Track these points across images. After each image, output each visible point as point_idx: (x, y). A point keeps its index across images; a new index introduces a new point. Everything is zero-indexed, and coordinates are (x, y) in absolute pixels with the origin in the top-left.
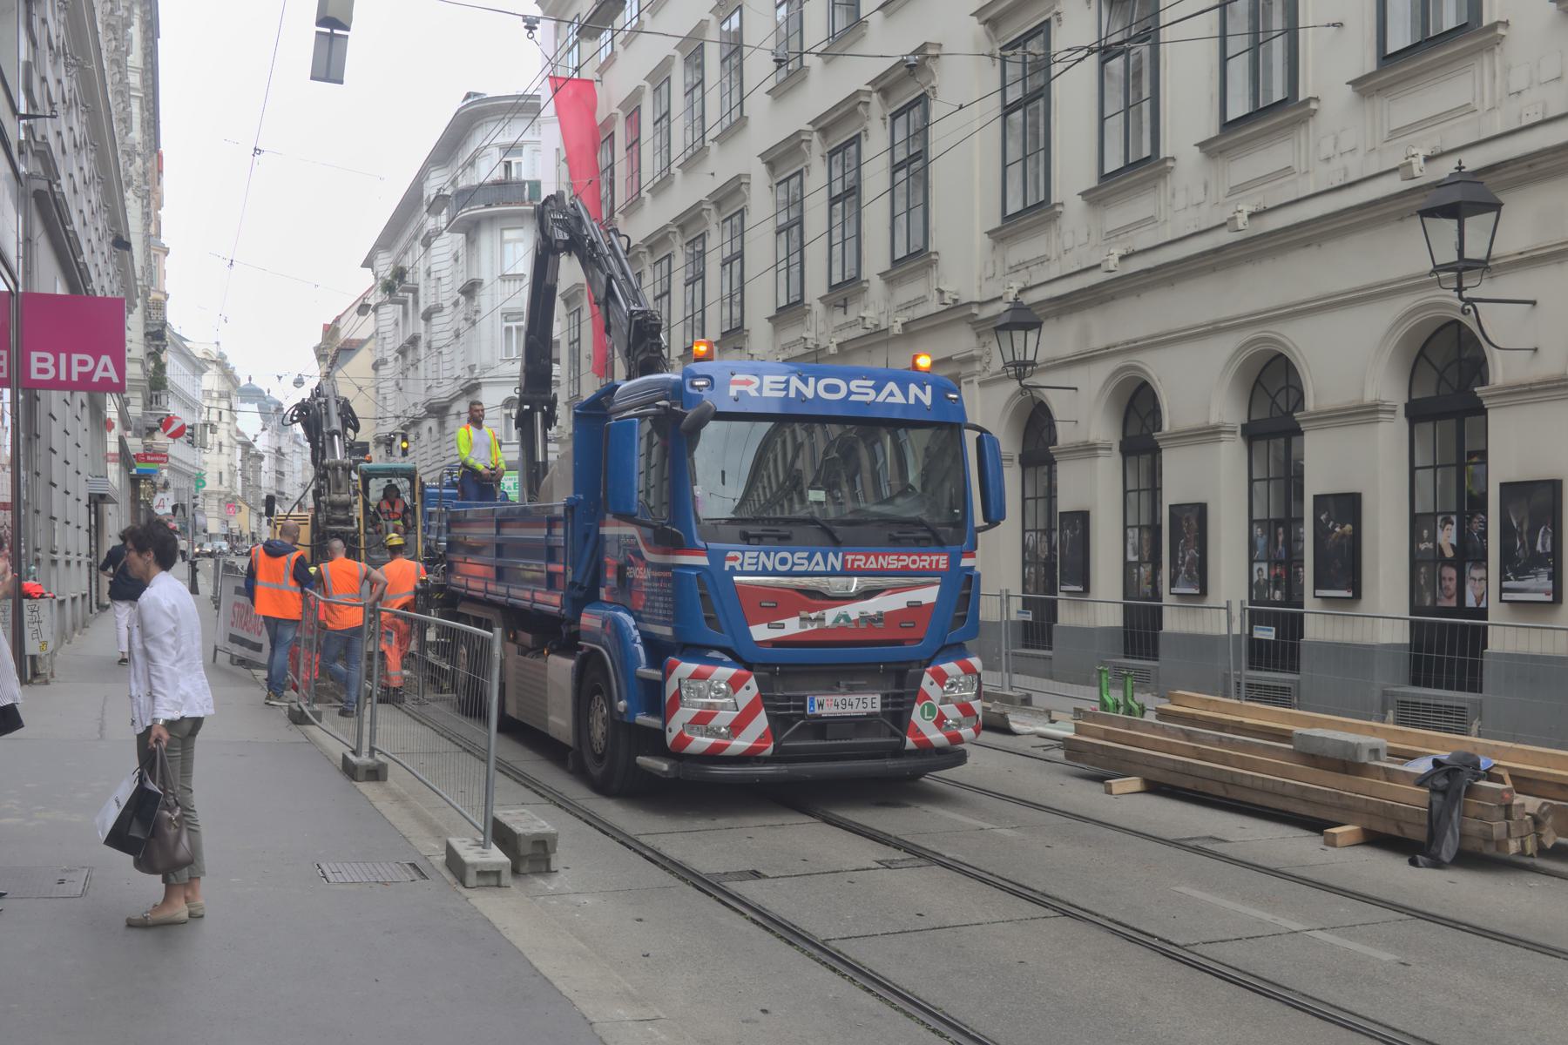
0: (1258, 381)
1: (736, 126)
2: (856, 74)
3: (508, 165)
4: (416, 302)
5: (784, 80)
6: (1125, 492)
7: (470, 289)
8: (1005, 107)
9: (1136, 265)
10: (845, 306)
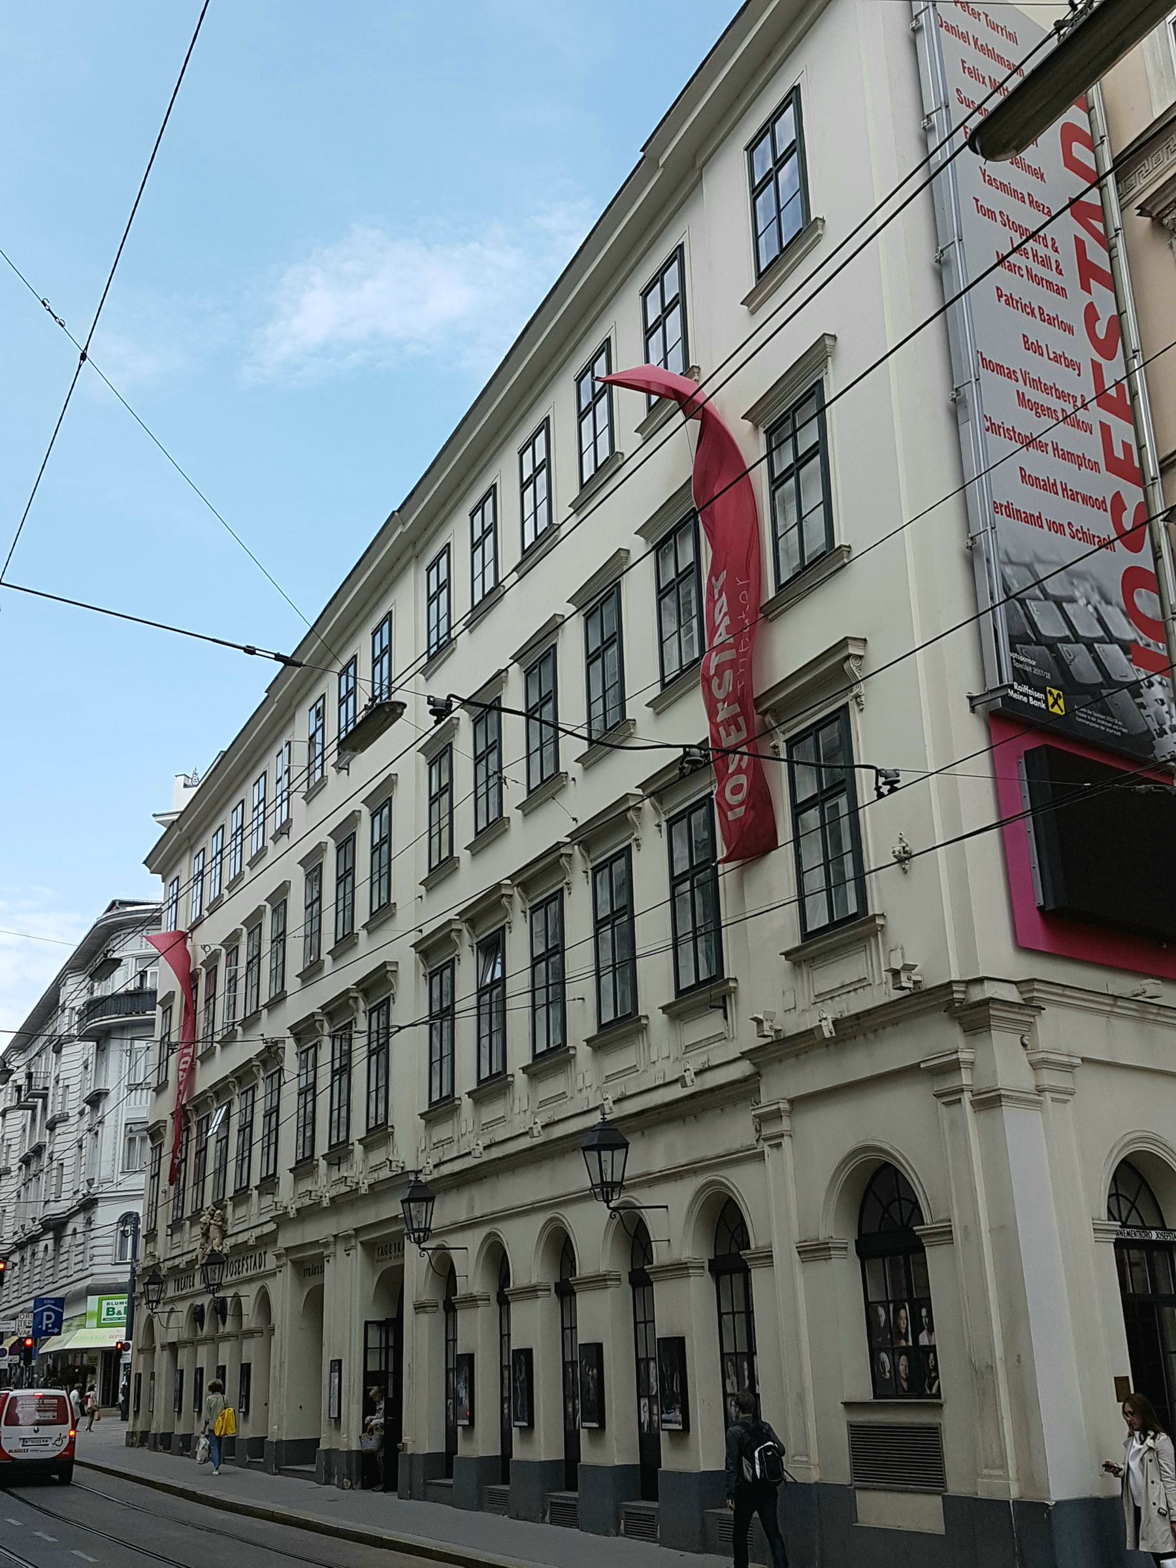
0: (869, 1188)
1: (383, 913)
2: (554, 825)
3: (143, 975)
4: (45, 1108)
5: (309, 967)
6: (720, 1315)
7: (95, 1100)
8: (533, 959)
9: (496, 1153)
10: (339, 1164)
